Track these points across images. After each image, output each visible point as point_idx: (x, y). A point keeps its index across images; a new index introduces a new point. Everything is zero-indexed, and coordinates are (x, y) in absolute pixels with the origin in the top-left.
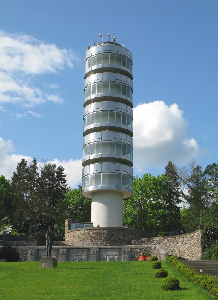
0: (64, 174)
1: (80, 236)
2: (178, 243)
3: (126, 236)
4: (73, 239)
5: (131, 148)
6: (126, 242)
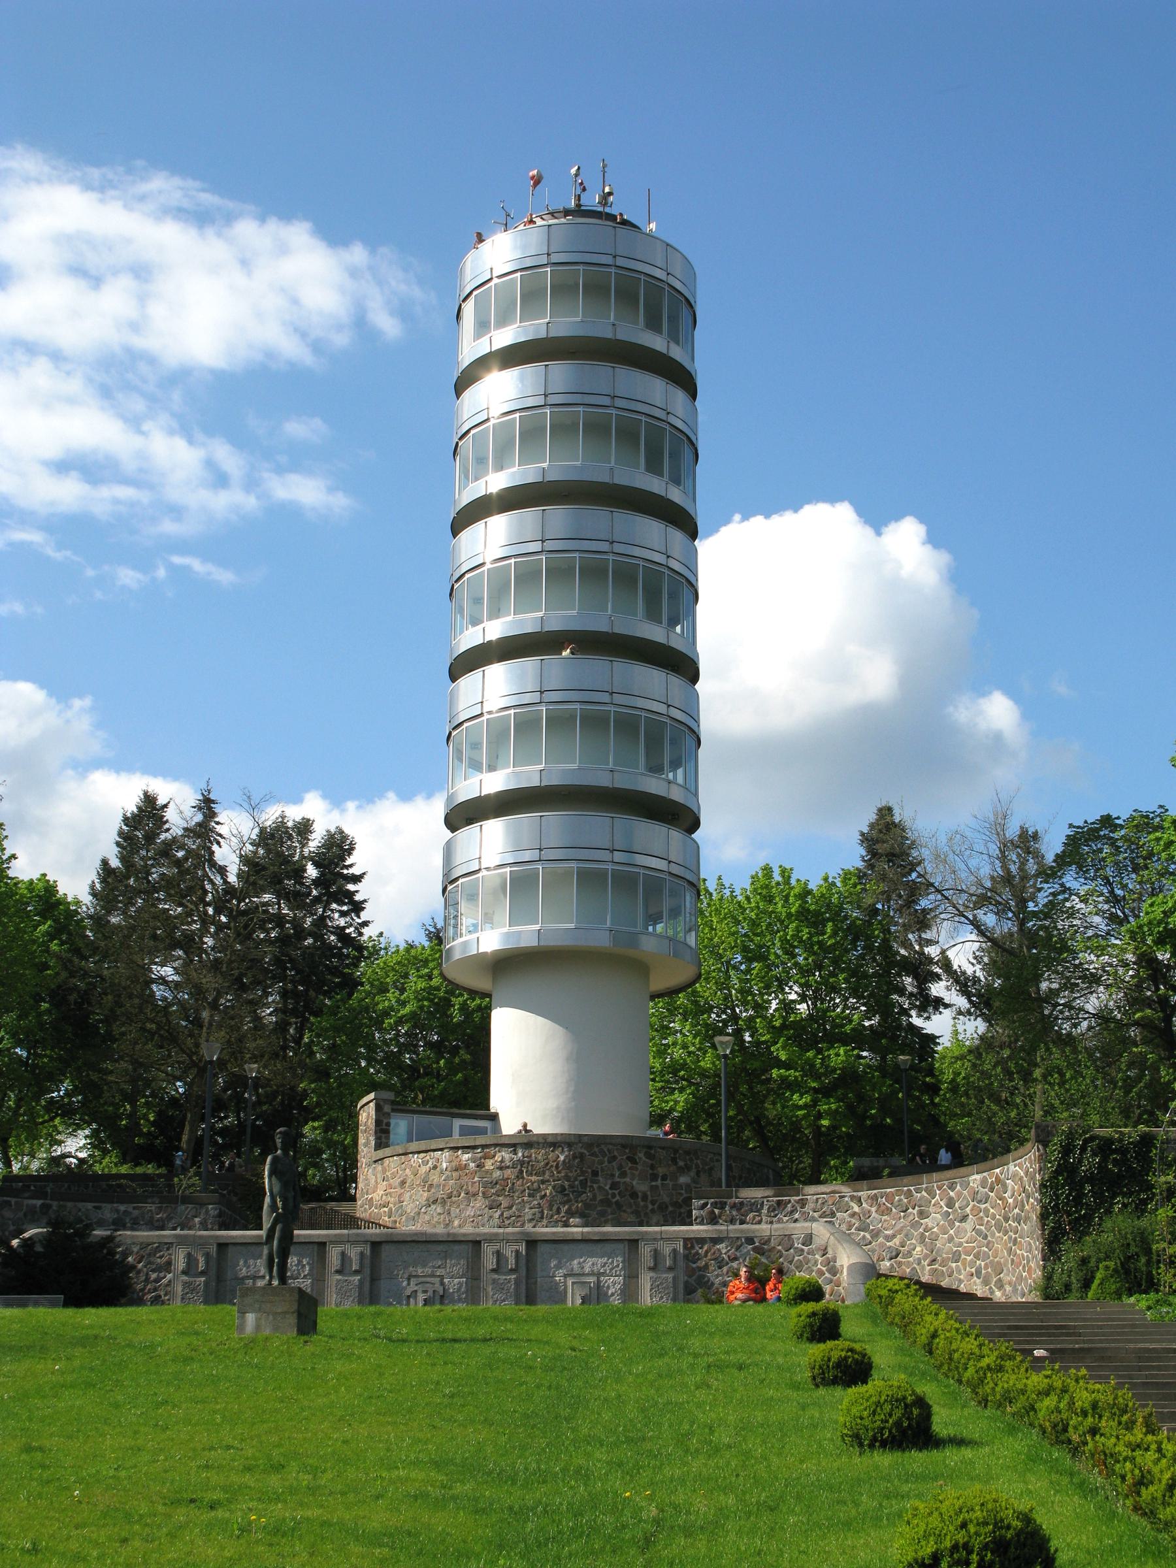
0: (355, 871)
1: (435, 1178)
2: (923, 1214)
3: (664, 1178)
6: (663, 1208)
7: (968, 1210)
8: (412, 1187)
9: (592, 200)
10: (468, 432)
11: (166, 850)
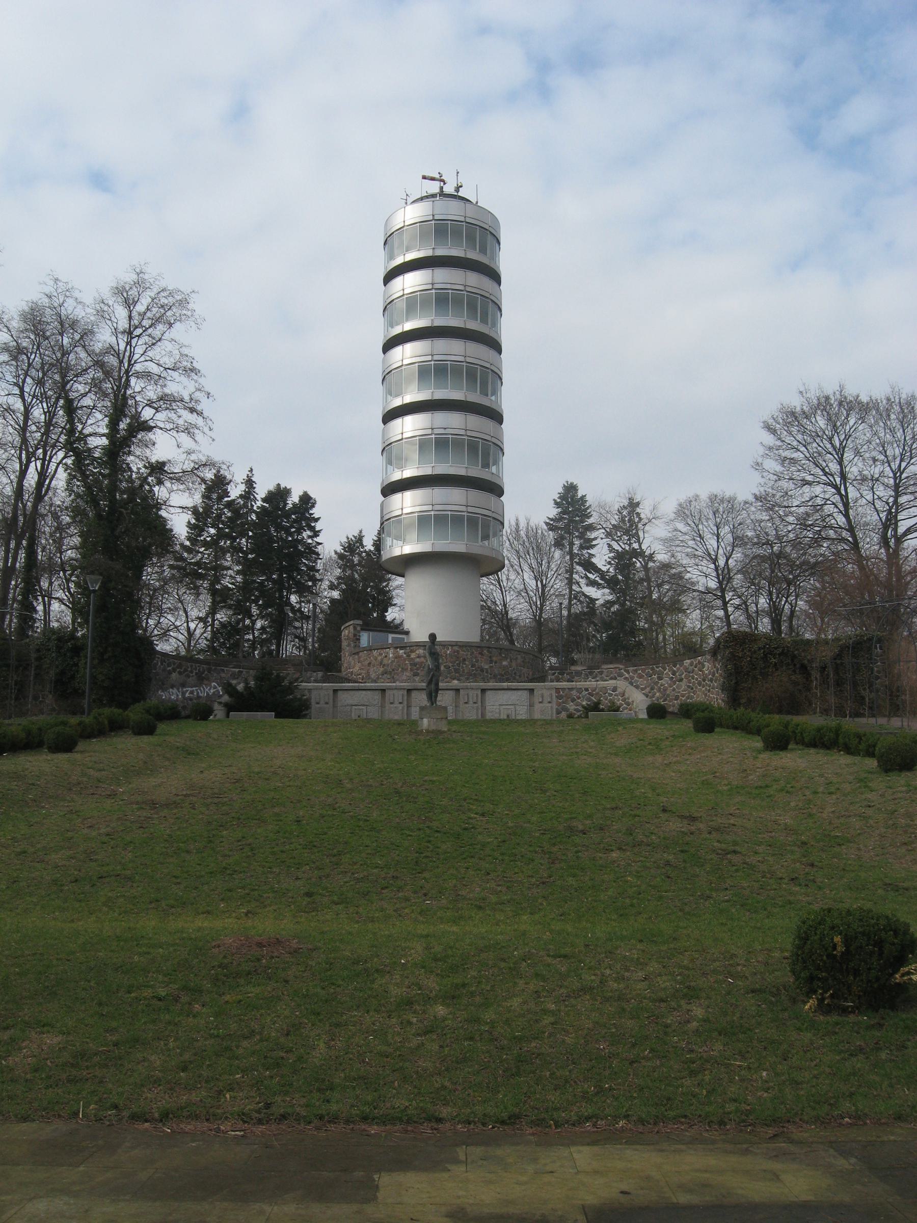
0: (316, 516)
1: (385, 661)
2: (660, 678)
3: (496, 663)
4: (368, 670)
5: (501, 454)
6: (495, 676)
7: (683, 676)
8: (374, 666)
9: (449, 189)
10: (393, 301)
11: (230, 504)
